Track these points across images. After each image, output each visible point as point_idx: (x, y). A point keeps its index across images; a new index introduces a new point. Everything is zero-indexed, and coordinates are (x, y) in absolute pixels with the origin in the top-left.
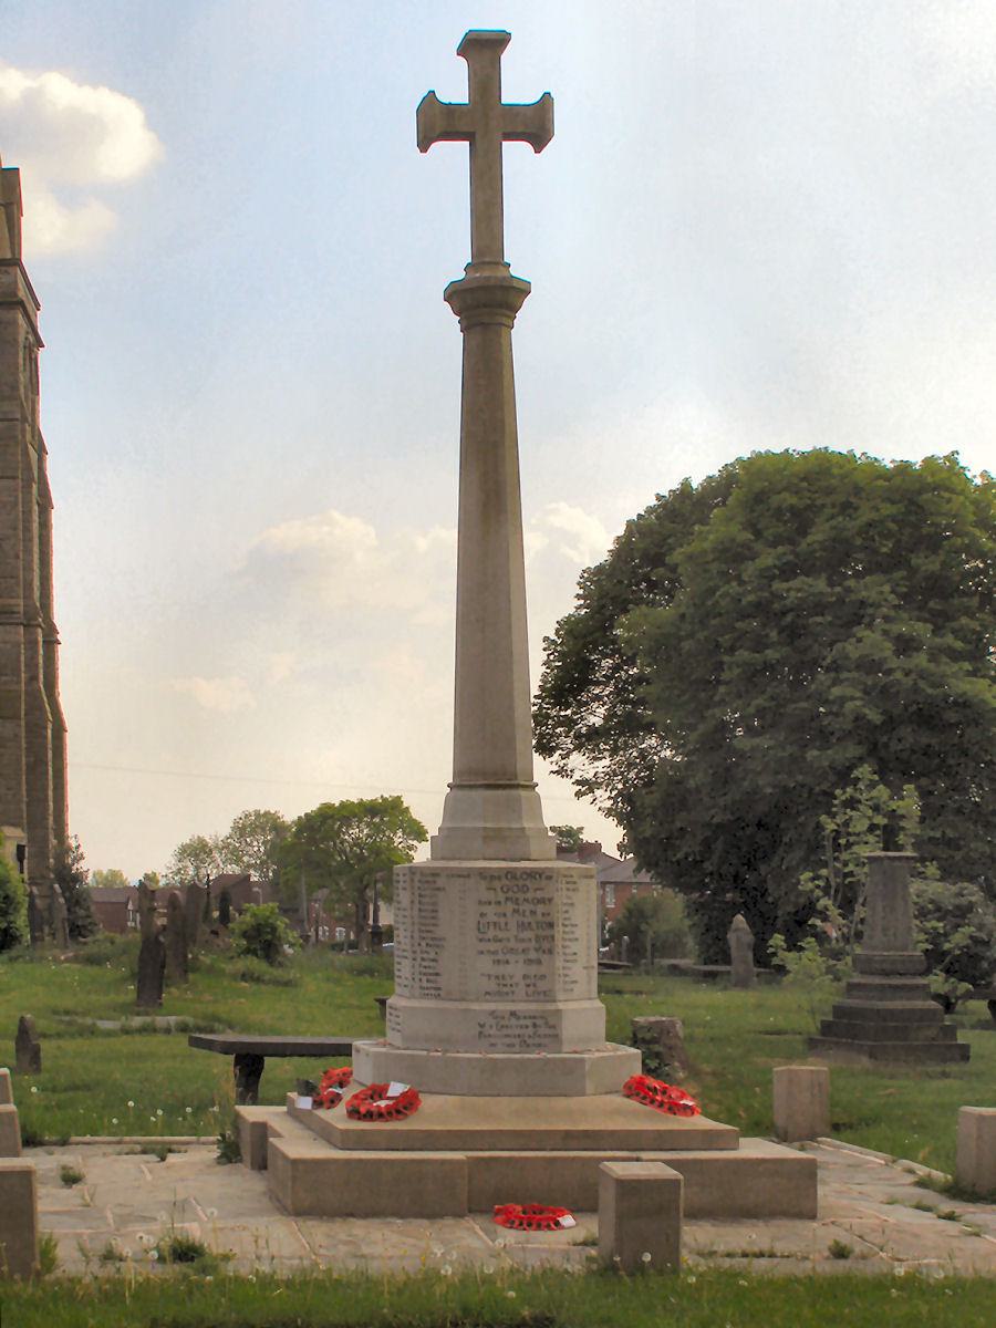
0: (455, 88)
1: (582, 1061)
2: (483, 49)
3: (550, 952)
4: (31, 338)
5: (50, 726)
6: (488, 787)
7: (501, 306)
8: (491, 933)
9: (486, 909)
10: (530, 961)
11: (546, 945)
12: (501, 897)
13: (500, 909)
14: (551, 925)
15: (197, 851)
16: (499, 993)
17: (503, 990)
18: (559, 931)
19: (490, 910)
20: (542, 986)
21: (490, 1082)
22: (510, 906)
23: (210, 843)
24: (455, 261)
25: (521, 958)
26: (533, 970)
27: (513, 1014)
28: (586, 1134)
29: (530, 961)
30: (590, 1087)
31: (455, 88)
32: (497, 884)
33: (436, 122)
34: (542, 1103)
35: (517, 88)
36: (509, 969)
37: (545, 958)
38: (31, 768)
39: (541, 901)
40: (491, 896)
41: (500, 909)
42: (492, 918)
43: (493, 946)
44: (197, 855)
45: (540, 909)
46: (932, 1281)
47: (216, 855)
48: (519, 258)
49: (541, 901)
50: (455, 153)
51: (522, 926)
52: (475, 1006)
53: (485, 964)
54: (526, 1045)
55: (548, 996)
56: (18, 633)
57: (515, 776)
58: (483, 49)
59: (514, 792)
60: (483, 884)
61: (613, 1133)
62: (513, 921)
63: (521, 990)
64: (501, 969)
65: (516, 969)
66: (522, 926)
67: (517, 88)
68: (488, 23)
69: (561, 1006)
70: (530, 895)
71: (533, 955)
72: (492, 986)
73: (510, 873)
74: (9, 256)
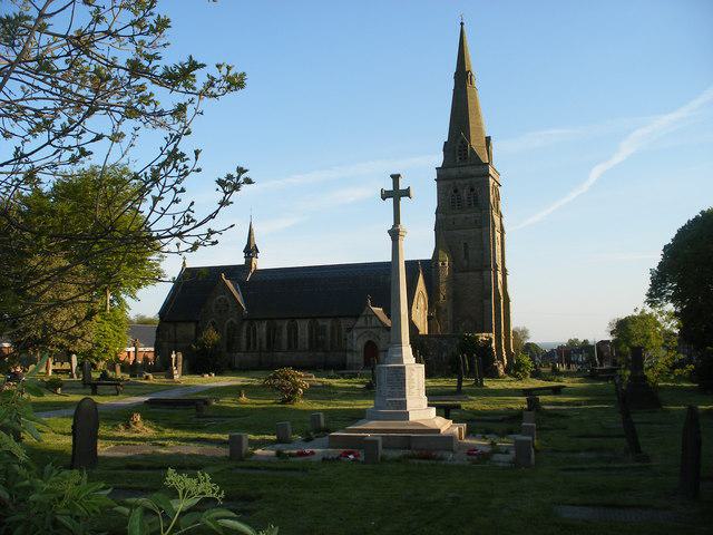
0: (389, 187)
2: (396, 178)
58: (396, 178)
67: (402, 186)
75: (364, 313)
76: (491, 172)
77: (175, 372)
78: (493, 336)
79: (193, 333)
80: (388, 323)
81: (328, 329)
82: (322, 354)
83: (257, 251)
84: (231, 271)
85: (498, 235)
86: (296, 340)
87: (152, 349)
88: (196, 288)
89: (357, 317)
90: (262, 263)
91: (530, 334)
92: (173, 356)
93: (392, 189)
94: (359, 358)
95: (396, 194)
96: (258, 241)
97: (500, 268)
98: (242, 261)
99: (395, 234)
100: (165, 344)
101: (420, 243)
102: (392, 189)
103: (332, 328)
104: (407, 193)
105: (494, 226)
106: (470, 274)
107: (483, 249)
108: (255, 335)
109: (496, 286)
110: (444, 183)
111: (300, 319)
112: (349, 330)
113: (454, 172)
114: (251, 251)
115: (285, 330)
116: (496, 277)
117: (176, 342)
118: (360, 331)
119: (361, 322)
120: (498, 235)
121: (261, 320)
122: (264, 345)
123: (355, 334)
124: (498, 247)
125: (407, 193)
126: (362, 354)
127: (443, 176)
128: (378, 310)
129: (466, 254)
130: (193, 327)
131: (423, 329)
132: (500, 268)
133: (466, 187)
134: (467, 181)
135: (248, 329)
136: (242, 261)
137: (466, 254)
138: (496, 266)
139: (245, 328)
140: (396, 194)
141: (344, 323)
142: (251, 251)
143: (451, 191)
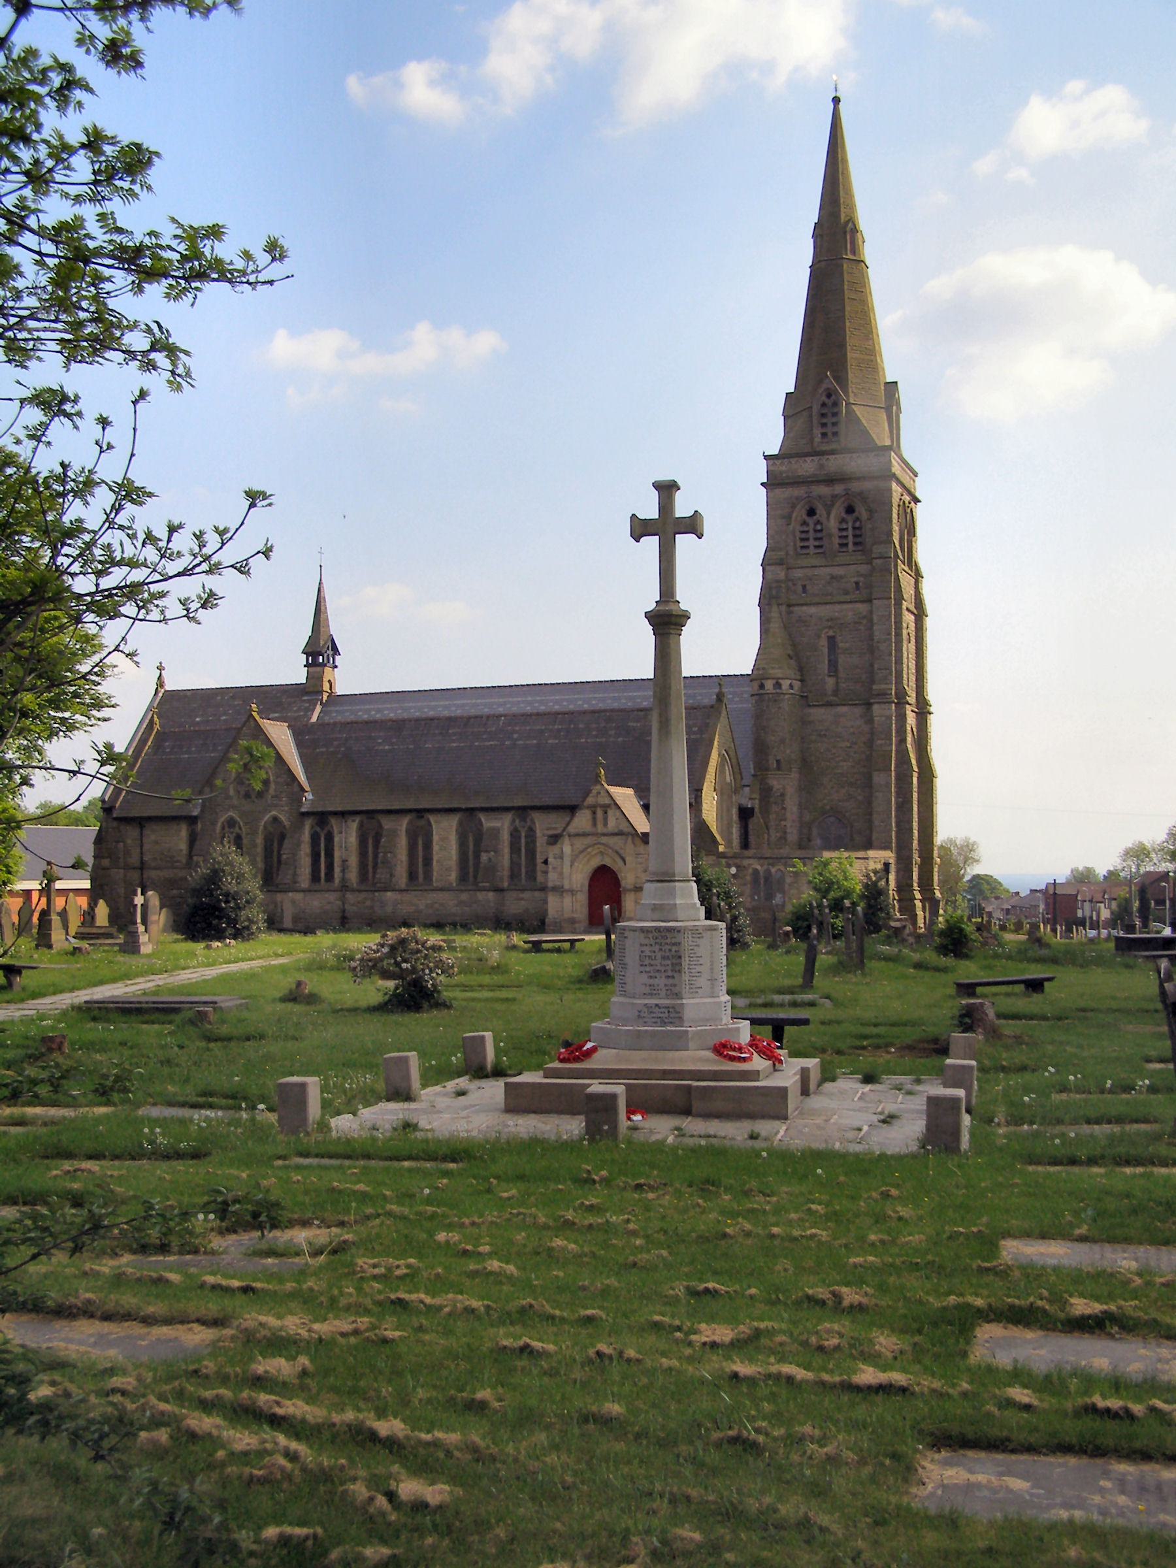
0: (650, 511)
1: (687, 1031)
2: (666, 490)
3: (680, 971)
4: (907, 498)
5: (915, 775)
6: (658, 881)
7: (676, 624)
8: (647, 962)
9: (644, 948)
10: (668, 977)
11: (677, 968)
12: (652, 942)
13: (653, 948)
14: (680, 957)
15: (1139, 853)
16: (651, 994)
17: (652, 992)
18: (685, 963)
19: (646, 949)
20: (676, 990)
21: (636, 1042)
22: (657, 948)
23: (1148, 845)
24: (650, 598)
25: (663, 975)
26: (671, 981)
27: (657, 1005)
28: (675, 1071)
29: (668, 977)
30: (691, 1044)
31: (650, 511)
32: (650, 935)
33: (640, 529)
34: (660, 1054)
35: (682, 508)
36: (656, 981)
37: (676, 975)
38: (900, 807)
39: (674, 944)
40: (647, 941)
41: (653, 948)
42: (648, 953)
43: (648, 969)
44: (1137, 857)
45: (674, 948)
46: (575, 1138)
47: (1153, 855)
48: (685, 597)
49: (674, 944)
50: (651, 544)
51: (664, 958)
52: (638, 1001)
53: (644, 978)
54: (664, 1024)
55: (678, 996)
56: (890, 709)
57: (674, 875)
58: (666, 490)
59: (672, 884)
60: (642, 935)
61: (618, 1070)
62: (659, 955)
63: (663, 993)
64: (651, 981)
65: (661, 981)
66: (664, 958)
67: (682, 508)
68: (665, 476)
69: (684, 1001)
70: (668, 941)
71: (670, 974)
72: (647, 990)
73: (657, 929)
74: (888, 443)
75: (590, 800)
76: (896, 468)
77: (143, 938)
78: (889, 856)
79: (183, 846)
80: (641, 824)
81: (505, 836)
82: (491, 895)
83: (336, 651)
84: (274, 698)
85: (909, 619)
86: (428, 861)
87: (86, 884)
88: (194, 727)
89: (572, 809)
90: (347, 679)
91: (982, 851)
92: (139, 900)
93: (655, 515)
94: (574, 905)
95: (666, 526)
96: (337, 628)
97: (912, 699)
98: (297, 674)
99: (667, 622)
100: (118, 874)
101: (725, 639)
102: (655, 515)
103: (514, 834)
104: (693, 525)
105: (900, 598)
106: (373, 1163)
107: (872, 650)
108: (330, 854)
109: (902, 741)
110: (778, 491)
111: (379, 813)
112: (554, 839)
113: (807, 467)
114: (320, 651)
115: (403, 842)
116: (902, 718)
117: (142, 867)
118: (580, 843)
119: (582, 821)
120: (909, 619)
121: (343, 814)
122: (353, 876)
123: (567, 849)
124: (909, 649)
125: (693, 525)
126: (582, 898)
127: (780, 477)
128: (624, 796)
129: (833, 665)
130: (184, 831)
131: (589, 1090)
132: (912, 699)
133: (839, 520)
134: (839, 489)
135: (315, 839)
136: (297, 674)
137: (833, 665)
138: (902, 695)
139: (306, 836)
140: (666, 526)
141: (543, 824)
142: (320, 651)
143: (800, 513)
